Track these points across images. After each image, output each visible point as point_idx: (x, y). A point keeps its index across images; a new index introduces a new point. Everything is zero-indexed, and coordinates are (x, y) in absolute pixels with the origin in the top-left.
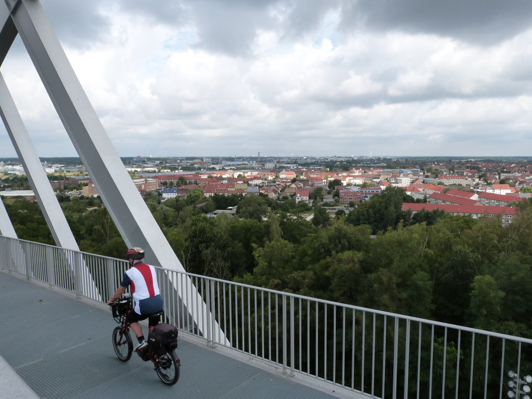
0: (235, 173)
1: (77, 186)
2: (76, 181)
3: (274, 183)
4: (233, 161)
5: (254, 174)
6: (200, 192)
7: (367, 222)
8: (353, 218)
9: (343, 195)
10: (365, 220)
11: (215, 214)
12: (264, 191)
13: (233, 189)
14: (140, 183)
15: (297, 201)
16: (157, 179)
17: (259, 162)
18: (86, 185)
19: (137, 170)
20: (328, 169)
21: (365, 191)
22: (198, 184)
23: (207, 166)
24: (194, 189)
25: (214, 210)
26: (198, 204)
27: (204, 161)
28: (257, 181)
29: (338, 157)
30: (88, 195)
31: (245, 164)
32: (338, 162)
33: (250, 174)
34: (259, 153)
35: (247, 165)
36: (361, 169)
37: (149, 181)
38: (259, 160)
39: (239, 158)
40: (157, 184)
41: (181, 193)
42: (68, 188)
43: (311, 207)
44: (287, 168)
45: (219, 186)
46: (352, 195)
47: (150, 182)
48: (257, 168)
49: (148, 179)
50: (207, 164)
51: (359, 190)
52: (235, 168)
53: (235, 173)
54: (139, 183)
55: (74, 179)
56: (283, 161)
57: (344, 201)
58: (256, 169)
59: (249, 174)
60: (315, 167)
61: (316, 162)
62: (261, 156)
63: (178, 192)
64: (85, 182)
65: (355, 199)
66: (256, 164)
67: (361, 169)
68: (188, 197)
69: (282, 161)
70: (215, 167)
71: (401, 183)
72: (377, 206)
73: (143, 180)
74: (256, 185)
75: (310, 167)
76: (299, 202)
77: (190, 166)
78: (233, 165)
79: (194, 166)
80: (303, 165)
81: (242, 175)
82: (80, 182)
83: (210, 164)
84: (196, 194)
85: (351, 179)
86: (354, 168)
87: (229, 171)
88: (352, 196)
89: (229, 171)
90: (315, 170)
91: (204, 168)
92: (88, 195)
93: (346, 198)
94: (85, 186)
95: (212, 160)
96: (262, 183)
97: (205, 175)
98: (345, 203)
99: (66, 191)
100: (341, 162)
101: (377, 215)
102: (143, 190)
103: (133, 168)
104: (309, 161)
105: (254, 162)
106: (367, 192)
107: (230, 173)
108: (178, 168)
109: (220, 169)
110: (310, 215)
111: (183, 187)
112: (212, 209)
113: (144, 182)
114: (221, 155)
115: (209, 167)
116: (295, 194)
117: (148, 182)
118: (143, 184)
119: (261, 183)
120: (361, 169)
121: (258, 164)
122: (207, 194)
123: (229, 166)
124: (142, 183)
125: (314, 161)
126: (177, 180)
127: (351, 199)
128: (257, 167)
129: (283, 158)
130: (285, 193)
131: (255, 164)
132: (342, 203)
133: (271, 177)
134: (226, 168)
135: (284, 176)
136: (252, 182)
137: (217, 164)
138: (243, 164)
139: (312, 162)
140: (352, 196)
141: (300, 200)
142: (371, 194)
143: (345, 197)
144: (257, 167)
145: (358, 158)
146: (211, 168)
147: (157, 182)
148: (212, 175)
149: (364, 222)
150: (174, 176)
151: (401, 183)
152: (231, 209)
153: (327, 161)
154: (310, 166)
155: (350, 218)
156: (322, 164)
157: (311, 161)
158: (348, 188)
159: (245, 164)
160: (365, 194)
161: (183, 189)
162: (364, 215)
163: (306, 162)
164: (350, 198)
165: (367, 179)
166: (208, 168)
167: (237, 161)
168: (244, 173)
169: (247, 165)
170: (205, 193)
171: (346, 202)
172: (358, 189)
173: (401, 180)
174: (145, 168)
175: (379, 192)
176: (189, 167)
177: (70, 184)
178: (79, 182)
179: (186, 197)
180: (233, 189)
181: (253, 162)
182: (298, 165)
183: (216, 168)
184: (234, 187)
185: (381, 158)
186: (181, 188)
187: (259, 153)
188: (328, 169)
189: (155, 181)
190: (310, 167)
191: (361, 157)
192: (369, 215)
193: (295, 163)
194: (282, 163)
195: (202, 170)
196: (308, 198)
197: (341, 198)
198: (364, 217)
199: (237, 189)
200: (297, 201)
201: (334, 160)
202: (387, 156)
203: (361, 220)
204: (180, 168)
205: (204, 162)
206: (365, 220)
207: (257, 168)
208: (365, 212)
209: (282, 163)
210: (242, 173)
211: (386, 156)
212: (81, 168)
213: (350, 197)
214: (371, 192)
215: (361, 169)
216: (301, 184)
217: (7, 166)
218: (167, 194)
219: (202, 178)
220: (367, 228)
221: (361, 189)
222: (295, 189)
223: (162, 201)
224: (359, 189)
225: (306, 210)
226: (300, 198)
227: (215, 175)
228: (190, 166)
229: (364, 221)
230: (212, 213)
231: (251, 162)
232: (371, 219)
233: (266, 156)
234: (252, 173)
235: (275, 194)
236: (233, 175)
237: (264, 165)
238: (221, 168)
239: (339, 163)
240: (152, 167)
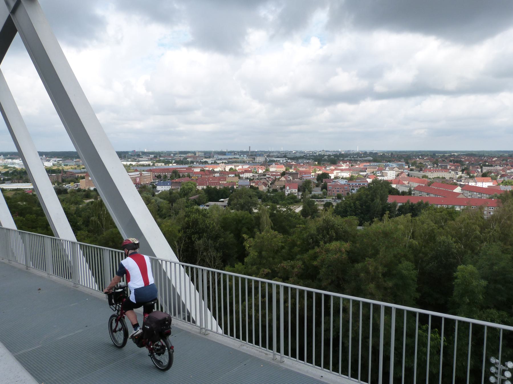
0: (227, 167)
1: (74, 179)
2: (73, 174)
3: (264, 176)
4: (225, 155)
5: (245, 168)
6: (193, 185)
7: (354, 213)
8: (341, 210)
9: (331, 188)
10: (352, 212)
11: (208, 206)
12: (255, 184)
14: (135, 176)
15: (287, 193)
16: (152, 172)
17: (250, 156)
18: (83, 178)
19: (132, 164)
20: (317, 163)
21: (352, 184)
22: (191, 177)
24: (187, 182)
26: (191, 197)
27: (197, 155)
28: (247, 174)
29: (326, 151)
30: (85, 187)
31: (236, 158)
32: (326, 156)
33: (241, 168)
34: (250, 147)
35: (238, 158)
36: (348, 162)
37: (144, 174)
38: (250, 154)
39: (231, 153)
40: (152, 177)
41: (174, 185)
42: (65, 181)
45: (211, 179)
46: (340, 188)
47: (145, 175)
48: (248, 162)
49: (143, 172)
51: (346, 183)
52: (227, 162)
53: (227, 167)
54: (134, 176)
55: (71, 173)
56: (273, 155)
57: (332, 194)
58: (247, 163)
59: (240, 167)
60: (304, 161)
61: (304, 156)
62: (252, 150)
63: (171, 185)
64: (82, 175)
65: (343, 191)
66: (247, 158)
68: (181, 189)
69: (272, 155)
70: (207, 161)
71: (387, 176)
72: (364, 199)
73: (138, 173)
74: (247, 178)
75: (299, 161)
76: (289, 195)
77: (184, 160)
78: (225, 159)
79: (187, 159)
80: (292, 159)
81: (233, 168)
82: (77, 175)
84: (189, 187)
86: (341, 162)
87: (221, 165)
88: (340, 189)
89: (221, 165)
90: (303, 164)
91: (197, 162)
92: (85, 187)
93: (333, 191)
94: (82, 179)
95: (204, 154)
96: (253, 176)
97: (197, 169)
98: (333, 195)
99: (64, 184)
101: (364, 207)
102: (138, 183)
103: (129, 161)
104: (298, 155)
105: (245, 156)
106: (354, 185)
107: (222, 166)
108: (172, 162)
109: (212, 163)
110: (299, 207)
111: (177, 180)
112: (204, 201)
113: (139, 175)
114: (213, 149)
115: (202, 161)
116: (284, 187)
117: (143, 175)
118: (138, 177)
119: (252, 176)
120: (348, 162)
121: (249, 158)
122: (200, 186)
123: (221, 159)
124: (137, 176)
125: (303, 155)
126: (171, 174)
127: (339, 191)
128: (248, 161)
129: (273, 152)
130: (275, 186)
131: (246, 157)
132: (330, 195)
133: (262, 171)
134: (218, 162)
135: (274, 170)
136: (243, 175)
137: (210, 157)
138: (234, 158)
139: (301, 156)
140: (340, 189)
141: (289, 192)
142: (357, 187)
143: (333, 190)
144: (248, 161)
145: (345, 153)
146: (204, 161)
147: (152, 175)
149: (351, 214)
150: (168, 170)
151: (387, 176)
152: (223, 201)
153: (315, 155)
154: (299, 159)
155: (338, 210)
156: (311, 158)
157: (300, 155)
158: (335, 181)
159: (236, 158)
160: (352, 187)
161: (176, 182)
162: (351, 207)
163: (295, 156)
164: (337, 191)
165: (354, 173)
166: (201, 161)
167: (229, 155)
168: (235, 166)
169: (238, 158)
170: (198, 185)
171: (333, 194)
172: (345, 182)
173: (387, 173)
174: (140, 162)
176: (183, 161)
177: (68, 177)
178: (77, 176)
179: (179, 190)
180: (225, 182)
182: (287, 159)
183: (208, 162)
184: (225, 180)
185: (368, 152)
186: (174, 181)
187: (250, 147)
188: (317, 163)
189: (150, 174)
190: (299, 161)
191: (348, 151)
192: (356, 207)
193: (285, 157)
194: (272, 157)
195: (195, 163)
196: (297, 190)
198: (351, 209)
199: (228, 182)
200: (287, 193)
201: (322, 154)
202: (373, 150)
203: (348, 212)
204: (173, 162)
205: (197, 156)
206: (352, 212)
207: (248, 162)
208: (352, 204)
209: (272, 156)
210: (233, 167)
211: (373, 150)
212: (78, 162)
213: (338, 190)
214: (357, 185)
215: (348, 163)
216: (290, 177)
218: (161, 186)
219: (194, 171)
220: (354, 219)
221: (348, 182)
222: (284, 182)
223: (156, 193)
224: (346, 182)
225: (295, 202)
226: (289, 190)
227: (207, 168)
228: (184, 160)
229: (351, 213)
230: (205, 205)
231: (242, 156)
232: (358, 211)
233: (256, 151)
234: (243, 166)
235: (266, 186)
236: (225, 168)
237: (254, 159)
238: (213, 162)
239: (327, 157)
240: (147, 161)
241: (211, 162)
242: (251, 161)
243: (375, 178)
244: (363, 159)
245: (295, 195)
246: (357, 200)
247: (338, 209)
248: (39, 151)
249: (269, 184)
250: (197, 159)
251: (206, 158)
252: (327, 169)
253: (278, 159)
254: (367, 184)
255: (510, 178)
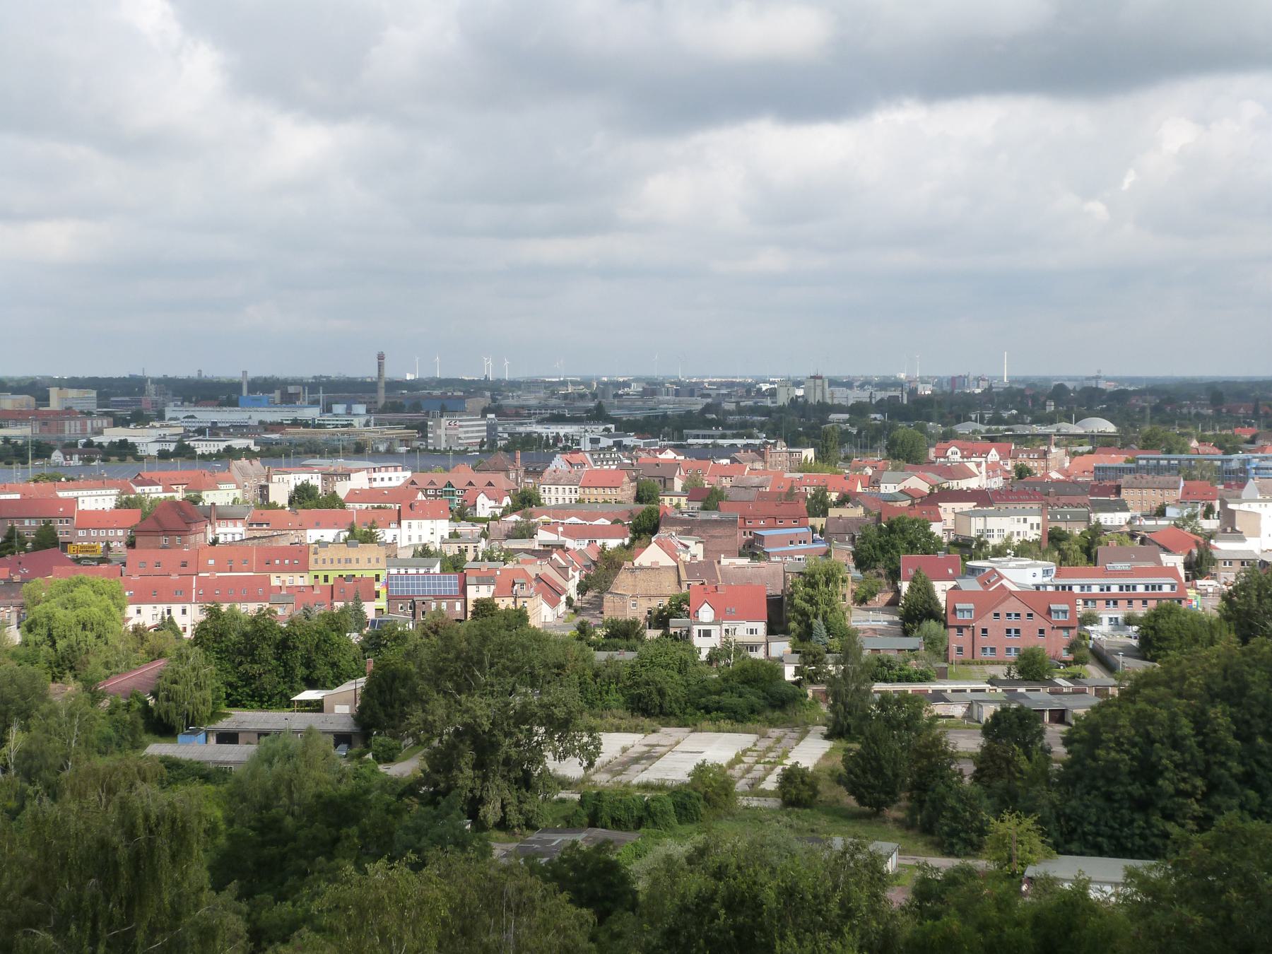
0: (275, 478)
3: (523, 537)
4: (233, 403)
5: (386, 484)
7: (1199, 782)
8: (1116, 761)
9: (969, 611)
10: (1186, 775)
11: (228, 738)
12: (492, 587)
13: (299, 580)
15: (704, 646)
17: (384, 410)
20: (809, 453)
21: (1082, 587)
23: (84, 430)
25: (216, 716)
27: (55, 404)
28: (420, 527)
29: (833, 383)
31: (306, 425)
32: (839, 409)
33: (366, 486)
34: (381, 357)
35: (320, 426)
36: (993, 451)
38: (382, 398)
39: (264, 387)
43: (798, 683)
44: (555, 445)
45: (211, 562)
46: (1024, 611)
48: (382, 448)
50: (84, 425)
51: (1047, 580)
52: (253, 447)
53: (275, 478)
56: (523, 407)
57: (978, 650)
58: (376, 451)
59: (359, 481)
60: (720, 442)
61: (708, 408)
62: (391, 373)
65: (1041, 632)
66: (367, 424)
67: (994, 455)
69: (516, 407)
70: (130, 440)
71: (1257, 534)
72: (1255, 690)
74: (425, 553)
75: (690, 441)
76: (713, 657)
78: (239, 430)
80: (652, 426)
81: (315, 488)
83: (98, 423)
85: (969, 515)
86: (954, 449)
87: (241, 469)
88: (1024, 615)
89: (241, 469)
90: (733, 460)
91: (69, 448)
93: (985, 631)
95: (99, 395)
96: (451, 536)
98: (980, 656)
100: (858, 410)
101: (1260, 740)
104: (668, 404)
105: (360, 409)
106: (1095, 589)
107: (245, 475)
109: (163, 455)
110: (801, 739)
112: (201, 707)
114: (154, 368)
115: (96, 440)
116: (680, 607)
119: (447, 536)
120: (993, 451)
121: (379, 423)
122: (144, 608)
123: (214, 431)
125: (700, 407)
127: (1017, 631)
128: (382, 441)
129: (514, 385)
130: (617, 599)
131: (363, 420)
132: (967, 656)
133: (492, 503)
134: (202, 447)
135: (567, 496)
136: (397, 531)
137: (140, 419)
138: (296, 423)
139: (689, 412)
140: (1024, 615)
141: (715, 640)
142: (1115, 603)
143: (979, 625)
144: (382, 441)
145: (938, 391)
146: (112, 444)
148: (138, 490)
149: (1182, 786)
151: (1257, 534)
152: (317, 706)
153: (768, 402)
154: (685, 431)
155: (1095, 759)
156: (753, 425)
157: (680, 403)
158: (982, 569)
159: (306, 425)
160: (1086, 603)
162: (1176, 743)
163: (652, 413)
164: (1009, 631)
165: (1064, 515)
166: (89, 444)
167: (257, 403)
168: (327, 476)
169: (320, 426)
171: (984, 649)
172: (1039, 571)
173: (1257, 516)
175: (1166, 589)
180: (299, 580)
181: (349, 412)
182: (612, 427)
183: (139, 449)
184: (304, 568)
185: (1070, 385)
187: (381, 357)
188: (809, 453)
190: (690, 441)
191: (953, 379)
192: (1209, 746)
193: (598, 415)
194: (518, 415)
195: (57, 456)
196: (761, 627)
197: (960, 629)
198: (1177, 756)
199: (321, 579)
200: (704, 646)
201: (811, 400)
202: (1097, 378)
203: (1161, 773)
205: (56, 413)
206: (1186, 775)
207: (382, 448)
208: (1184, 721)
209: (519, 413)
210: (316, 480)
211: (1094, 374)
213: (1013, 623)
214: (1115, 589)
215: (994, 455)
216: (691, 543)
217: (634, 741)
220: (251, 672)
221: (1056, 576)
222: (674, 578)
224: (1046, 573)
225: (773, 707)
226: (715, 630)
227: (153, 488)
229: (1184, 780)
230: (207, 733)
231: (339, 409)
232: (1222, 765)
233: (409, 377)
234: (375, 475)
235: (553, 604)
236: (267, 487)
237: (422, 429)
238: (172, 447)
239: (846, 416)
241: (158, 447)
242: (405, 441)
243: (1197, 543)
244: (1063, 431)
245: (753, 655)
246: (1213, 696)
247: (1101, 753)
248: (161, 376)
249: (571, 588)
250: (63, 431)
251: (124, 422)
252: (883, 490)
253: (563, 430)
254: (1173, 587)
255: (541, 473)
